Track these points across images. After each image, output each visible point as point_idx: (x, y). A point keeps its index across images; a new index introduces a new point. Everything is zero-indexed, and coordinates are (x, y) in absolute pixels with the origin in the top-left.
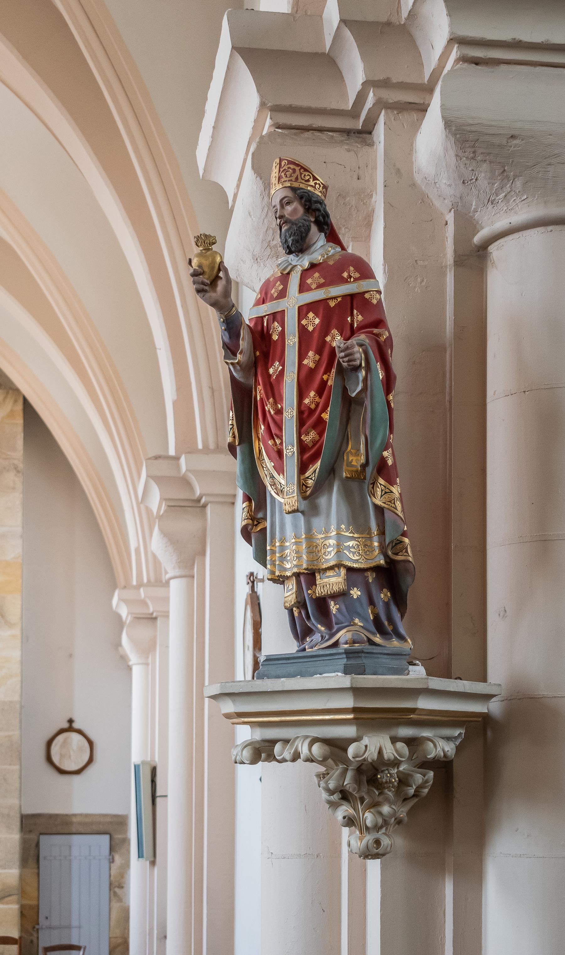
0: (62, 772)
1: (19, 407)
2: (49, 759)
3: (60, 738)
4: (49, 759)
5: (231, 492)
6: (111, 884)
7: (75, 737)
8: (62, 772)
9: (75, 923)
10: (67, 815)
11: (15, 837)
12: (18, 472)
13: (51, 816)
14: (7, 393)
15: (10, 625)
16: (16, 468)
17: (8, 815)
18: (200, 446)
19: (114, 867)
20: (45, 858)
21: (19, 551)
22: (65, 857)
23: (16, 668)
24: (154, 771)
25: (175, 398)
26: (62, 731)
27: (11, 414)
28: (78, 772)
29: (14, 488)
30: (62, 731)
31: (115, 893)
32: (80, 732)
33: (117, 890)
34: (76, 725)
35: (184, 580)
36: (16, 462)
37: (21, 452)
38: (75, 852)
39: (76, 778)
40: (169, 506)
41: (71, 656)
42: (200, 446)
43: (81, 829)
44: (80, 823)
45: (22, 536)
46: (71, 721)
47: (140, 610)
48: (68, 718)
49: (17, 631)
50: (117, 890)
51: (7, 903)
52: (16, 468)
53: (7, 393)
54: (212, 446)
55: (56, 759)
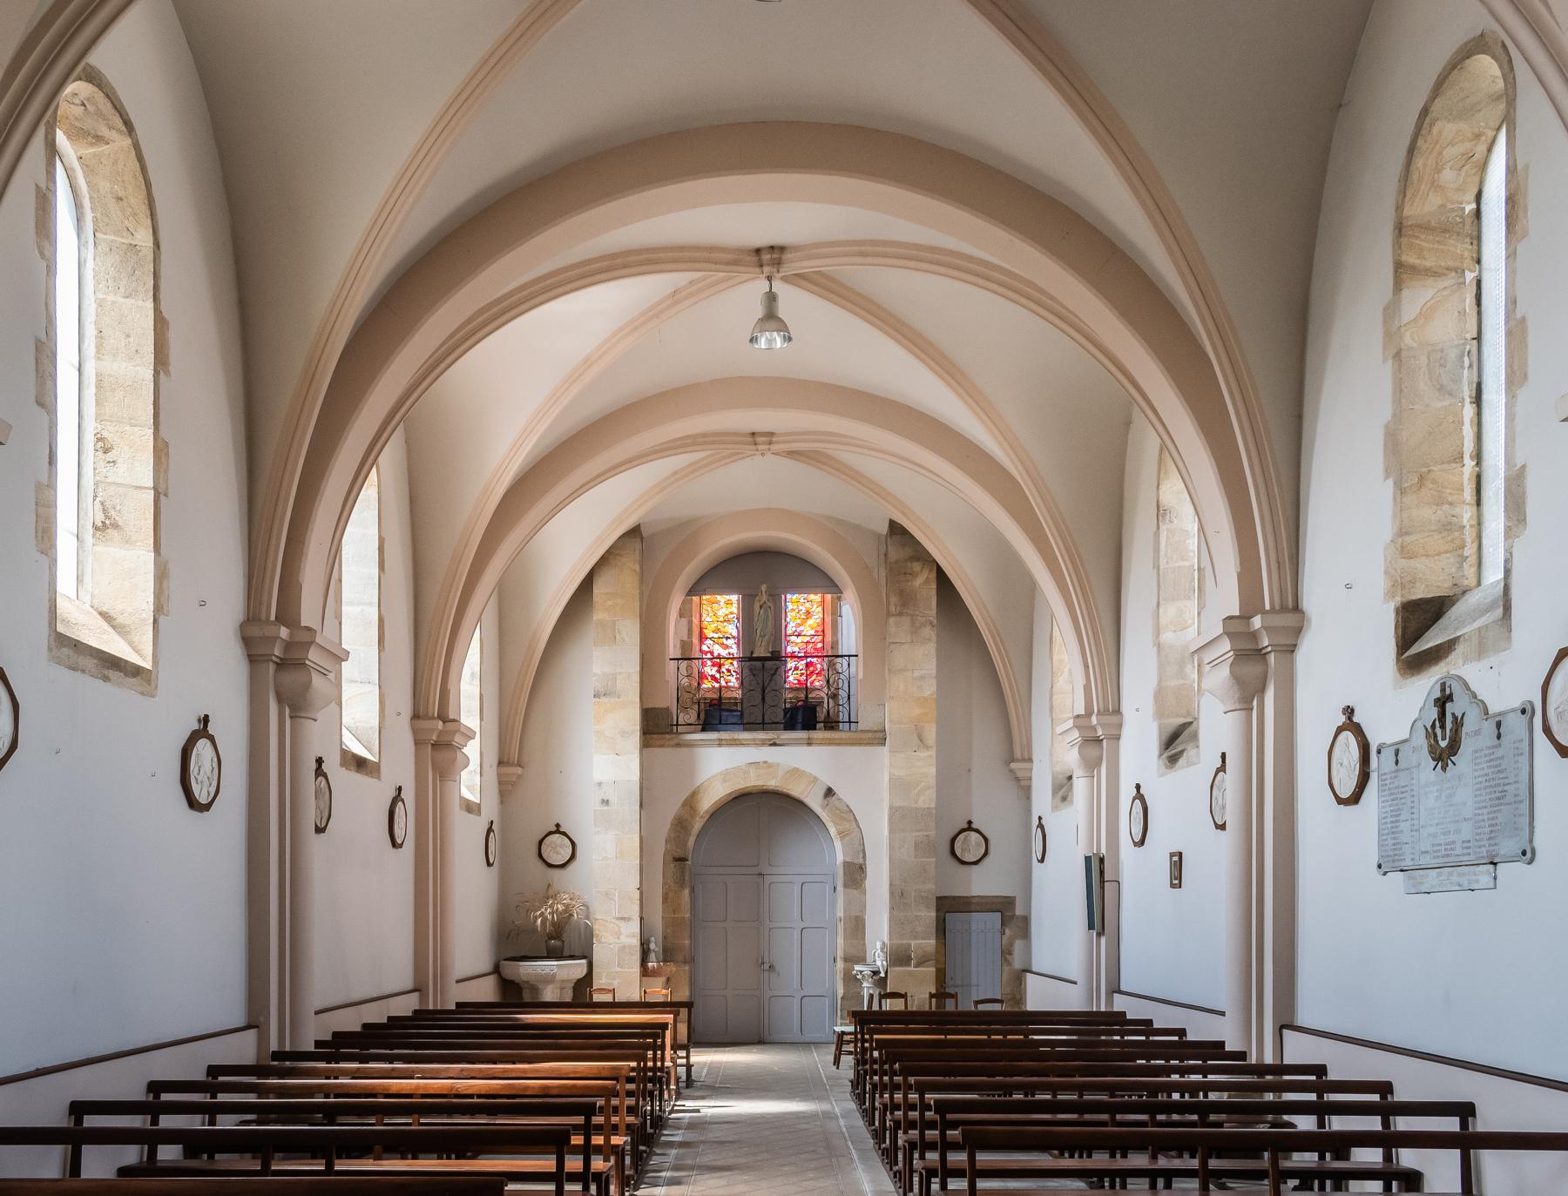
0: (963, 863)
1: (934, 575)
2: (953, 853)
3: (962, 836)
4: (953, 853)
5: (1293, 643)
6: (1002, 952)
7: (974, 835)
8: (963, 863)
9: (974, 981)
10: (967, 897)
11: (931, 914)
12: (933, 626)
13: (954, 898)
14: (924, 564)
15: (927, 747)
16: (931, 623)
17: (927, 897)
18: (1268, 607)
19: (1005, 938)
20: (950, 931)
21: (934, 688)
22: (966, 930)
23: (933, 781)
24: (1102, 860)
25: (1239, 570)
26: (963, 831)
27: (927, 581)
28: (976, 863)
29: (929, 639)
30: (963, 831)
31: (1005, 958)
32: (564, 834)
33: (1007, 956)
34: (974, 826)
35: (1243, 712)
36: (931, 618)
37: (934, 612)
38: (974, 926)
39: (974, 867)
40: (1237, 655)
41: (969, 771)
42: (1268, 607)
43: (978, 909)
44: (977, 903)
45: (936, 677)
46: (970, 822)
47: (1090, 734)
48: (967, 820)
49: (933, 752)
50: (1007, 956)
51: (927, 967)
52: (931, 623)
53: (924, 564)
54: (1277, 607)
55: (958, 853)
